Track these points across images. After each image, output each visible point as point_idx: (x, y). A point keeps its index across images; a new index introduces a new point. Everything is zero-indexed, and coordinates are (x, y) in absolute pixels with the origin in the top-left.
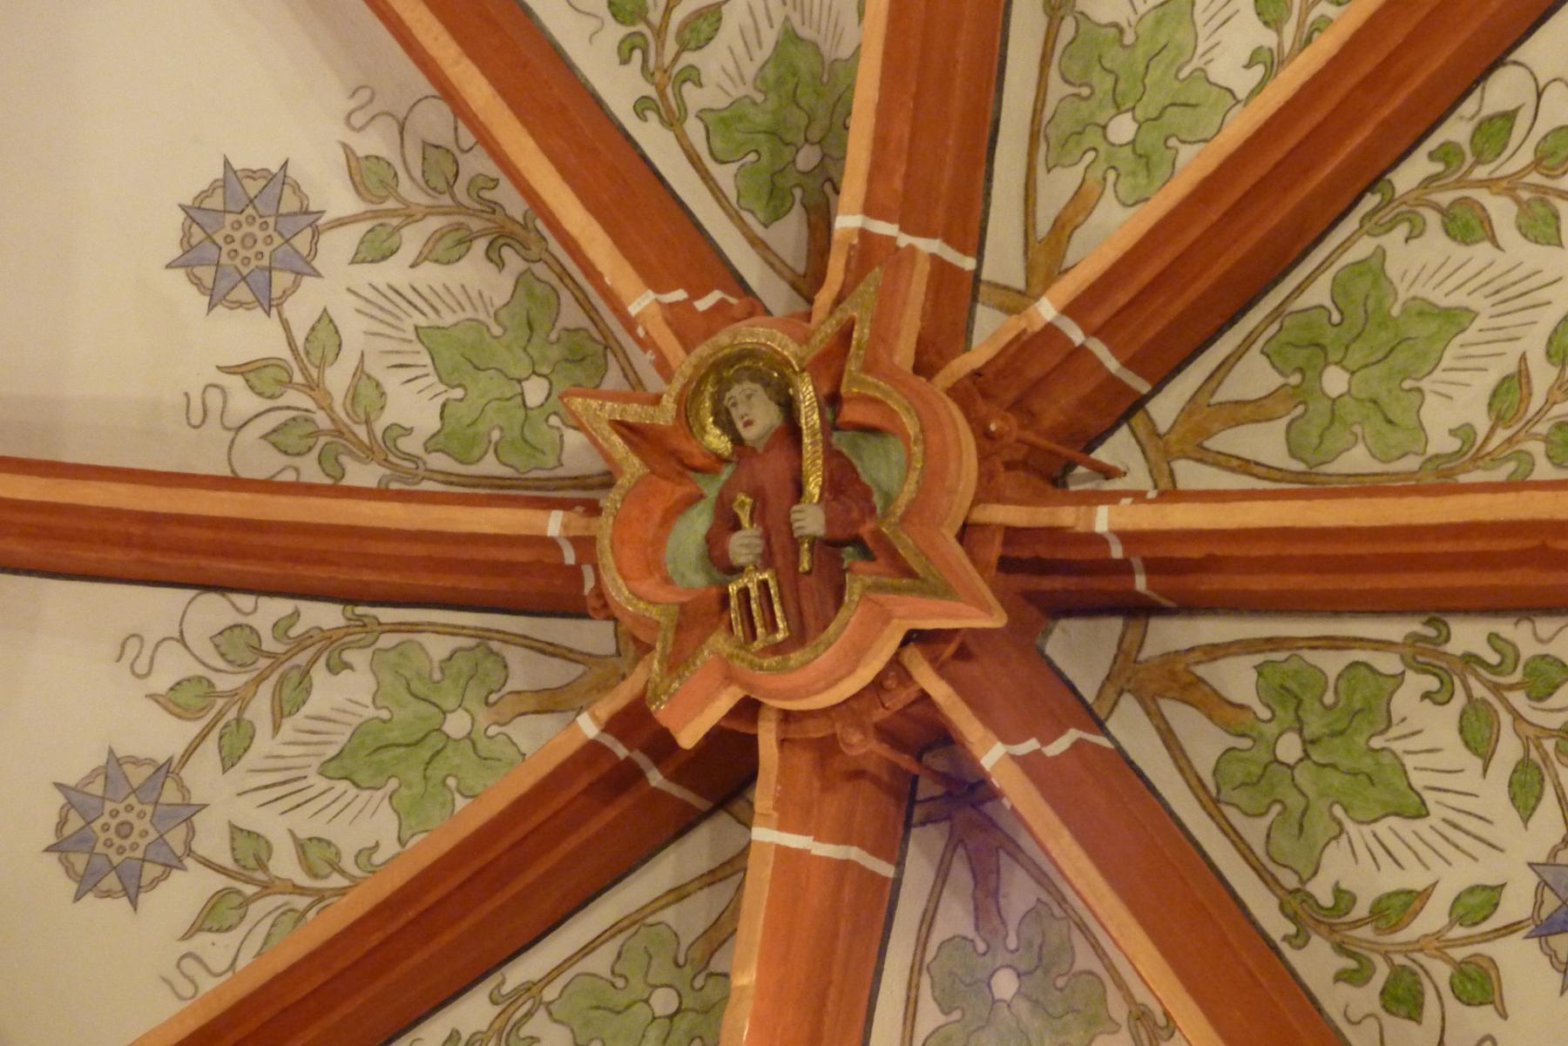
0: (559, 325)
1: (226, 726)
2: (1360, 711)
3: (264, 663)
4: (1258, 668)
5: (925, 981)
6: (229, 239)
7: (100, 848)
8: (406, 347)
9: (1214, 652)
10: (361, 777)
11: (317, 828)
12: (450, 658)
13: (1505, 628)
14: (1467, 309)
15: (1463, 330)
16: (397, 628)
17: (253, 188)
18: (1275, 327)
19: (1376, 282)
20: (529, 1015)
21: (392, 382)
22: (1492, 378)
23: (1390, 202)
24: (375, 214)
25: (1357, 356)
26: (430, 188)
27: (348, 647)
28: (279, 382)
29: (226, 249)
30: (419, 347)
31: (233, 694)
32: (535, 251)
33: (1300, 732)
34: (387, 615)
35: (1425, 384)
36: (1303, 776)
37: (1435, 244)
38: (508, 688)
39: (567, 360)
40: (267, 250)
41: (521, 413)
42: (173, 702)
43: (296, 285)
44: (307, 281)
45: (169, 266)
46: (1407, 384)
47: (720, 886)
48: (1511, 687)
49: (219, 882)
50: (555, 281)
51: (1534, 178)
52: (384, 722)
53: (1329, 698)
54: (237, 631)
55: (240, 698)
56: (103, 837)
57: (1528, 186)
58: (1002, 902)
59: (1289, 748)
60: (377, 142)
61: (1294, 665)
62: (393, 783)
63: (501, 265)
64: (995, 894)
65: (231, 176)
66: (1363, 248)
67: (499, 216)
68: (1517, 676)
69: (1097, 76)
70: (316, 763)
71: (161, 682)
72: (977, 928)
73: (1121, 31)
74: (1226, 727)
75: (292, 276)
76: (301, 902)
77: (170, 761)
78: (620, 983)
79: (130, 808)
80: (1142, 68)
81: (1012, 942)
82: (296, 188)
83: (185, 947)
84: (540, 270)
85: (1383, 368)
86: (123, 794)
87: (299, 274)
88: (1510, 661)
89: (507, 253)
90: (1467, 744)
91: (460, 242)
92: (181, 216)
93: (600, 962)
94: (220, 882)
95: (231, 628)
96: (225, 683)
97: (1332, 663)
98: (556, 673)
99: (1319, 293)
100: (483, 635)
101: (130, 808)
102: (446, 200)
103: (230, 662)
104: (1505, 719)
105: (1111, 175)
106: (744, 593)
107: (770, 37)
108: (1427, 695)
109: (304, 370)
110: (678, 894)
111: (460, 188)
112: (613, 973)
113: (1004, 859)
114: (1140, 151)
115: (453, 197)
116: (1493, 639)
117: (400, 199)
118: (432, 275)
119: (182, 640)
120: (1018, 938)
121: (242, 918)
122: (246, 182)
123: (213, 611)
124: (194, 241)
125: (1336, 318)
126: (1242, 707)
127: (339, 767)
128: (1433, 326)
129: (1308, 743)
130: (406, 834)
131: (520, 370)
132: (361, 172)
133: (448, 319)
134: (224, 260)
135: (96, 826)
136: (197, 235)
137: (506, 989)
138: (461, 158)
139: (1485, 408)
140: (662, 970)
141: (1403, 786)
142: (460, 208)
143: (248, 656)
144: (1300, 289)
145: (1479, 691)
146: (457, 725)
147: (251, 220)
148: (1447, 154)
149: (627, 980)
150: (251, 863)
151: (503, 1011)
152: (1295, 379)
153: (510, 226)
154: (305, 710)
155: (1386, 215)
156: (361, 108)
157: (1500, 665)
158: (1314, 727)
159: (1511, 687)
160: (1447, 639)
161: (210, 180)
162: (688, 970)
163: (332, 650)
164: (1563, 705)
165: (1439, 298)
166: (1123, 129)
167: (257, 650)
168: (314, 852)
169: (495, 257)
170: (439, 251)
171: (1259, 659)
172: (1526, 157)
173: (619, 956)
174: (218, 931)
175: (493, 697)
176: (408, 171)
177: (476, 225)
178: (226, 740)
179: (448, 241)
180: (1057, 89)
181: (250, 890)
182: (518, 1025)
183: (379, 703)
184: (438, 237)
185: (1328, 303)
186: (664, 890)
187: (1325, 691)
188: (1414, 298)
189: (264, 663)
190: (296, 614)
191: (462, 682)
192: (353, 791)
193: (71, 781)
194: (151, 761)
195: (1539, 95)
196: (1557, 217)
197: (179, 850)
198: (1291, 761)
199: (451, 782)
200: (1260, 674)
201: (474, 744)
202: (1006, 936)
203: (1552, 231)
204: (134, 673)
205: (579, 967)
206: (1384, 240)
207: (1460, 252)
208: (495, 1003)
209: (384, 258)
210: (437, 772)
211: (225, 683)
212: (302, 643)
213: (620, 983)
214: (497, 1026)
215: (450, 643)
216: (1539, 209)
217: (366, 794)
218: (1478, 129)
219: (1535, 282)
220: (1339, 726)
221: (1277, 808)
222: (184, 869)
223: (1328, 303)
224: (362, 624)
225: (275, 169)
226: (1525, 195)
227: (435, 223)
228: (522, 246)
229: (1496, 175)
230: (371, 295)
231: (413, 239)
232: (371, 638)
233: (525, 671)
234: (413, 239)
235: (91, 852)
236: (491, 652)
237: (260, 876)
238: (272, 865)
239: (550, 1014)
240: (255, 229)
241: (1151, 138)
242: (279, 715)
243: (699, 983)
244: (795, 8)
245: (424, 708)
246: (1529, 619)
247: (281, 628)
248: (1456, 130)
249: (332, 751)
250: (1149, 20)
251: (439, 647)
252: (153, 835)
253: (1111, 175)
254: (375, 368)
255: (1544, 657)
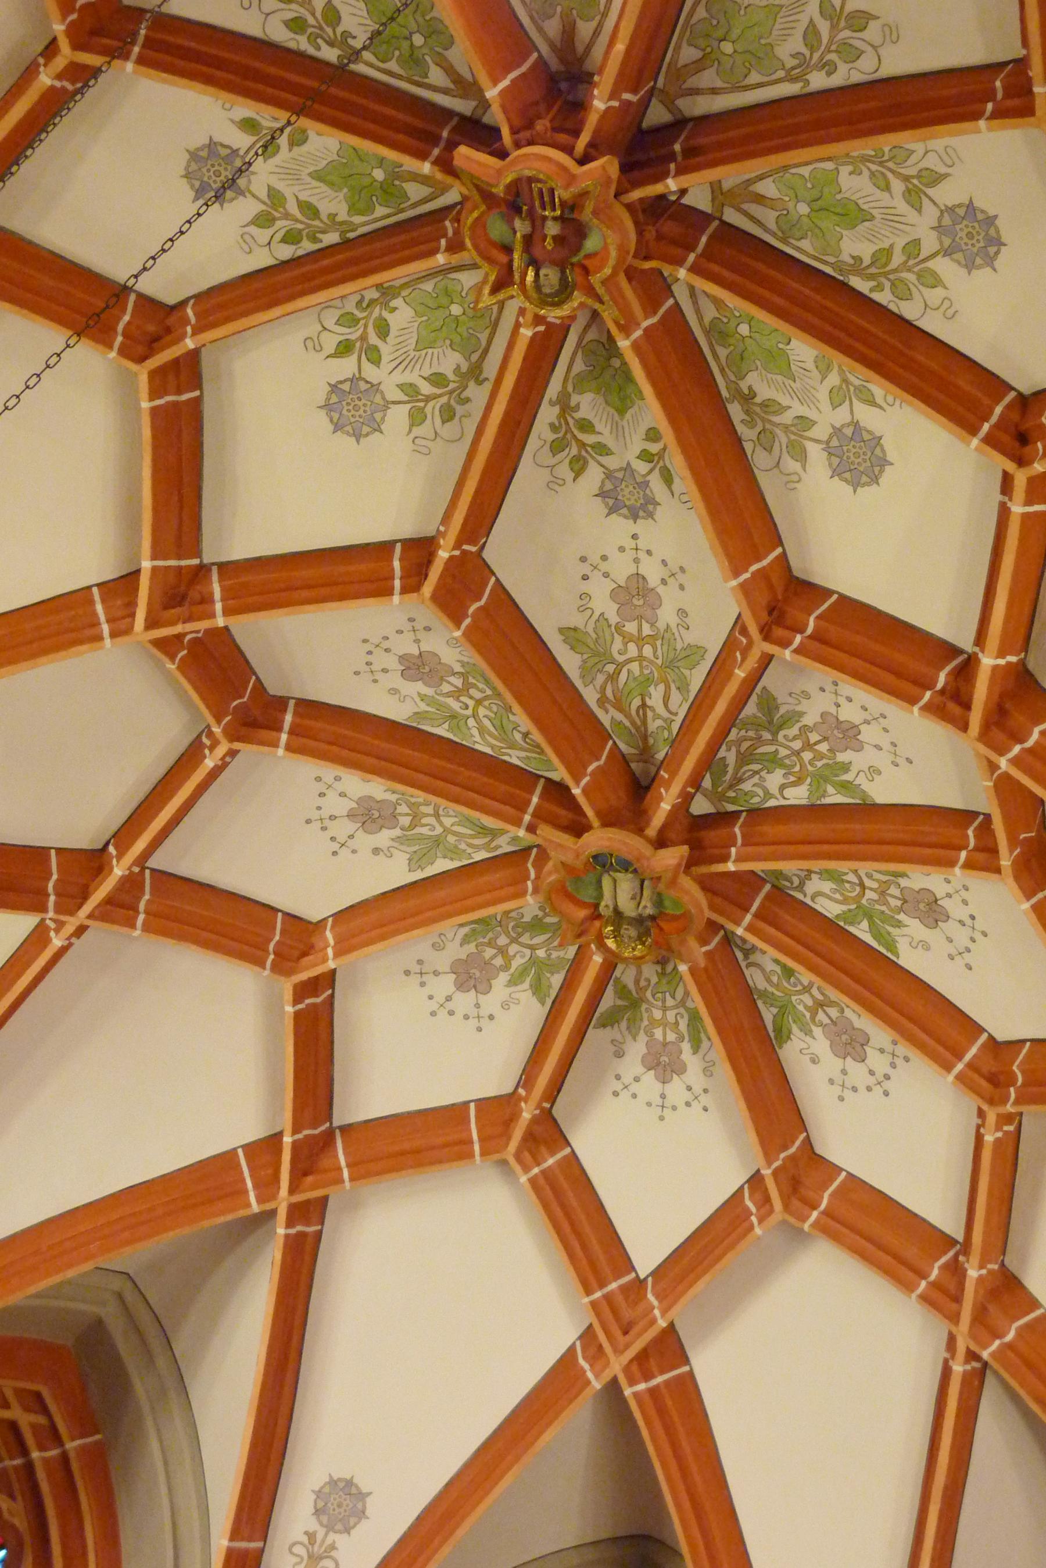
0: (728, 351)
1: (915, 258)
2: (384, 43)
3: (891, 277)
4: (427, 77)
5: (602, 8)
6: (865, 461)
7: (983, 234)
8: (801, 376)
9: (445, 91)
10: (852, 206)
11: (879, 194)
12: (801, 238)
13: (311, 51)
14: (313, 178)
15: (316, 171)
16: (825, 263)
17: (847, 475)
18: (402, 206)
19: (354, 205)
20: (793, 68)
21: (810, 365)
22: (305, 148)
23: (342, 232)
24: (801, 436)
25: (366, 181)
26: (774, 436)
27: (851, 265)
28: (860, 391)
29: (867, 457)
30: (795, 373)
31: (909, 270)
32: (733, 386)
33: (412, 45)
34: (828, 270)
35: (336, 157)
36: (414, 27)
37: (325, 207)
38: (778, 213)
39: (727, 336)
40: (850, 447)
41: (752, 324)
42: (936, 281)
43: (843, 426)
44: (838, 426)
45: (892, 464)
46: (345, 161)
47: (694, 86)
48: (313, 26)
49: (930, 191)
50: (727, 370)
51: (277, 215)
52: (838, 225)
53: (397, 53)
54: (900, 296)
55: (904, 267)
56: (980, 237)
57: (279, 212)
58: (561, 27)
59: (418, 40)
60: (791, 465)
61: (411, 73)
62: (838, 197)
63: (750, 388)
64: (564, 32)
65: (856, 485)
66: (358, 219)
67: (746, 408)
68: (310, 30)
69: (465, 334)
70: (875, 222)
71: (939, 292)
72: (575, 21)
73: (451, 345)
74: (446, 60)
75: (843, 431)
76: (890, 164)
77: (944, 256)
78: (747, 64)
79: (966, 244)
80: (444, 328)
81: (559, 9)
82: (830, 465)
83: (949, 170)
84: (733, 378)
85: (355, 171)
86: (969, 252)
87: (840, 430)
88: (312, 38)
89: (746, 392)
90: (338, 12)
91: (767, 406)
92: (880, 481)
93: (754, 78)
94: (930, 192)
95: (902, 299)
96: (911, 277)
97: (393, 65)
98: (753, 209)
99: (380, 211)
100: (784, 241)
101: (966, 244)
102: (768, 426)
103: (906, 284)
104: (318, 15)
105: (464, 294)
106: (554, 209)
107: (628, 416)
108: (355, 37)
109: (849, 391)
110: (714, 91)
111: (759, 428)
112: (750, 70)
113: (559, 45)
114: (450, 299)
115: (764, 426)
116: (319, 48)
117: (788, 438)
118: (784, 401)
119: (926, 305)
120: (556, 9)
121: (921, 170)
122: (850, 479)
123: (909, 310)
124: (879, 468)
125: (374, 198)
126: (437, 65)
127: (867, 217)
128: (328, 178)
129: (409, 38)
130: (835, 173)
131: (748, 341)
132: (802, 456)
133: (779, 378)
134: (869, 454)
135: (982, 244)
136: (877, 469)
137: (801, 84)
138: (755, 439)
139: (310, 138)
140: (727, 63)
141: (369, 6)
142: (763, 420)
143: (897, 283)
144: (389, 216)
145: (329, 30)
146: (803, 209)
147: (853, 463)
148: (314, 239)
149: (744, 64)
150: (913, 193)
151: (805, 75)
152: (397, 183)
153: (742, 401)
154: (877, 248)
155: (345, 227)
156: (794, 482)
157: (317, 38)
158: (405, 44)
159: (313, 26)
160: (339, 56)
161: (863, 489)
162: (713, 56)
163: (857, 266)
164: (622, 0)
165: (324, 188)
166: (456, 310)
167: (893, 284)
168: (882, 184)
169: (752, 393)
170: (777, 407)
171: (426, 80)
172: (279, 224)
173: (746, 76)
174: (933, 171)
175: (785, 212)
176: (781, 446)
177: (758, 409)
178: (916, 252)
179: (772, 409)
180: (484, 337)
181: (915, 181)
182: (799, 66)
183: (839, 235)
184: (776, 413)
185: (377, 206)
186: (721, 96)
187: (399, 57)
188: (336, 191)
189: (891, 277)
190: (871, 290)
191: (798, 226)
192: (860, 202)
193: (989, 269)
194: (952, 260)
195: (269, 243)
196: (268, 196)
197: (946, 214)
198: (418, 35)
199: (809, 185)
200: (427, 74)
201: (796, 196)
202: (561, 13)
203: (272, 192)
204: (950, 300)
205: (766, 79)
206: (347, 218)
207: (313, 200)
208: (807, 80)
209: (802, 417)
210: (815, 193)
211: (911, 277)
212: (872, 277)
213: (747, 64)
214: (809, 70)
215: (799, 244)
216: (276, 202)
217: (853, 198)
218: (299, 242)
219: (282, 176)
220: (394, 40)
221: (428, 18)
222: (946, 206)
223: (377, 206)
224: (841, 271)
225: (836, 478)
226: (281, 209)
227: (776, 419)
228: (739, 390)
229: (293, 222)
230: (812, 406)
231: (787, 418)
232: (839, 264)
233: (769, 217)
234: (787, 418)
235: (987, 234)
236: (783, 233)
237: (911, 186)
238: (904, 188)
239: (783, 65)
240: (852, 458)
241: (444, 301)
242: (889, 251)
243: (709, 50)
244: (617, 423)
245: (819, 223)
246: (299, 50)
247: (880, 288)
248: (307, 246)
249: (866, 224)
250: (439, 344)
251: (805, 244)
252: (958, 227)
253: (464, 294)
254: (816, 374)
255: (296, 33)
